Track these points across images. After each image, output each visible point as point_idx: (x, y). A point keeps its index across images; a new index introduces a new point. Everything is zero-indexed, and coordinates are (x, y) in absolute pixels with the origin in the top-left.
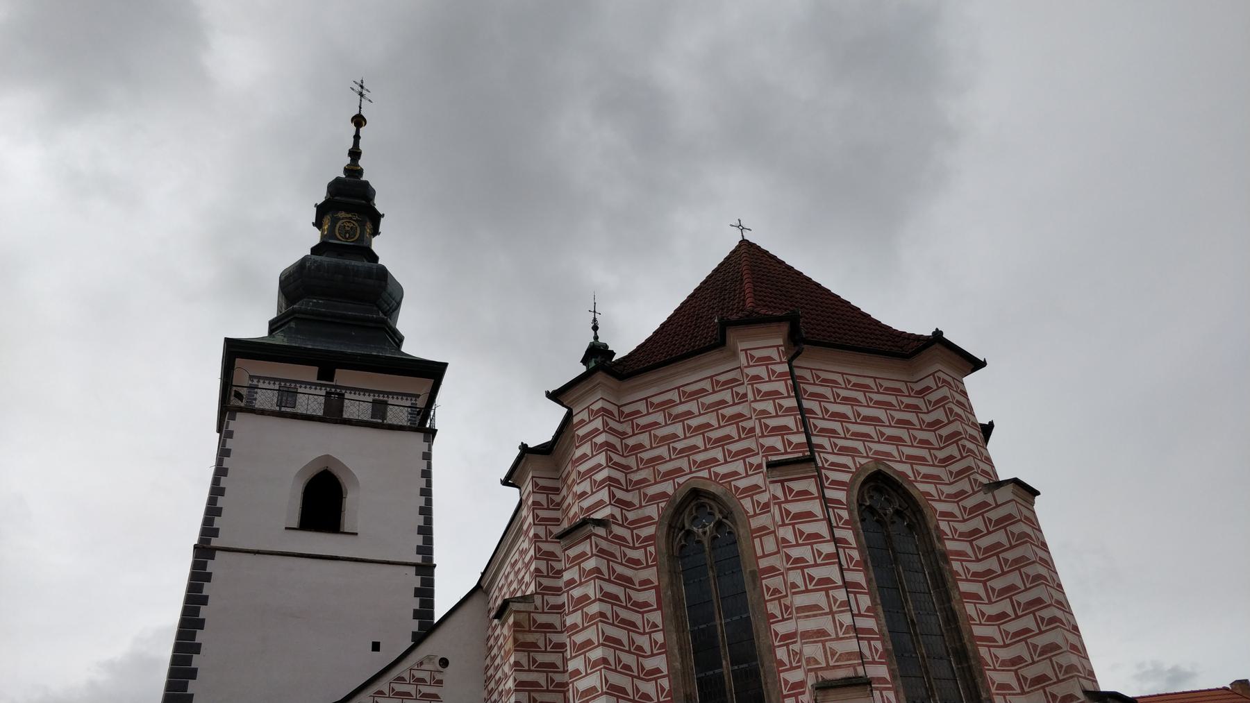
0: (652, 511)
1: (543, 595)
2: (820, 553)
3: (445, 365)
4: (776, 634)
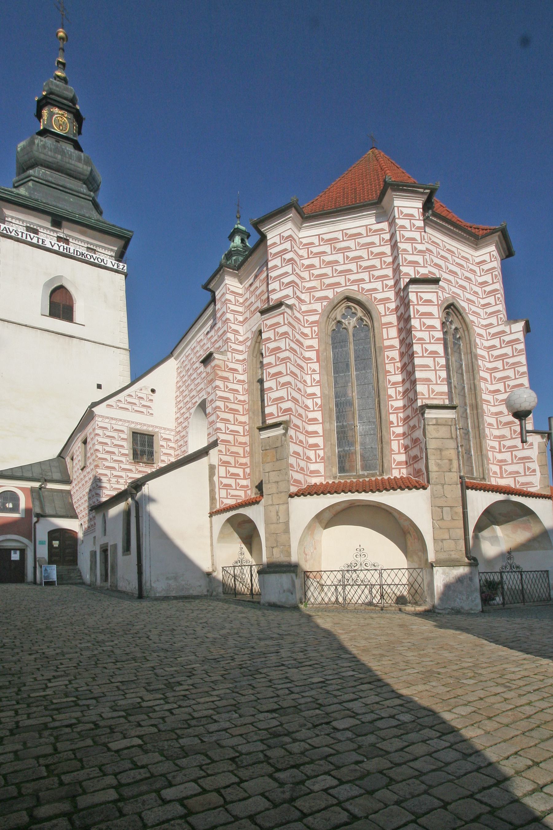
0: (318, 307)
2: (433, 337)
4: (390, 382)
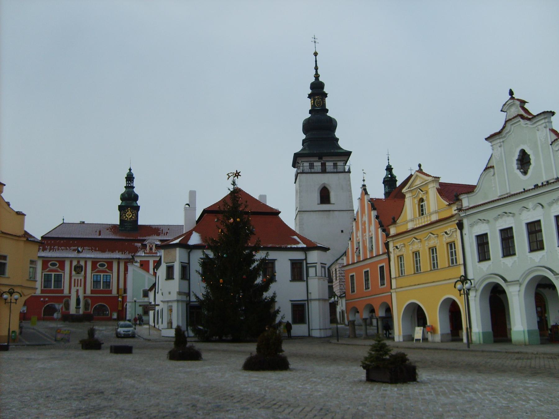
3: (351, 152)
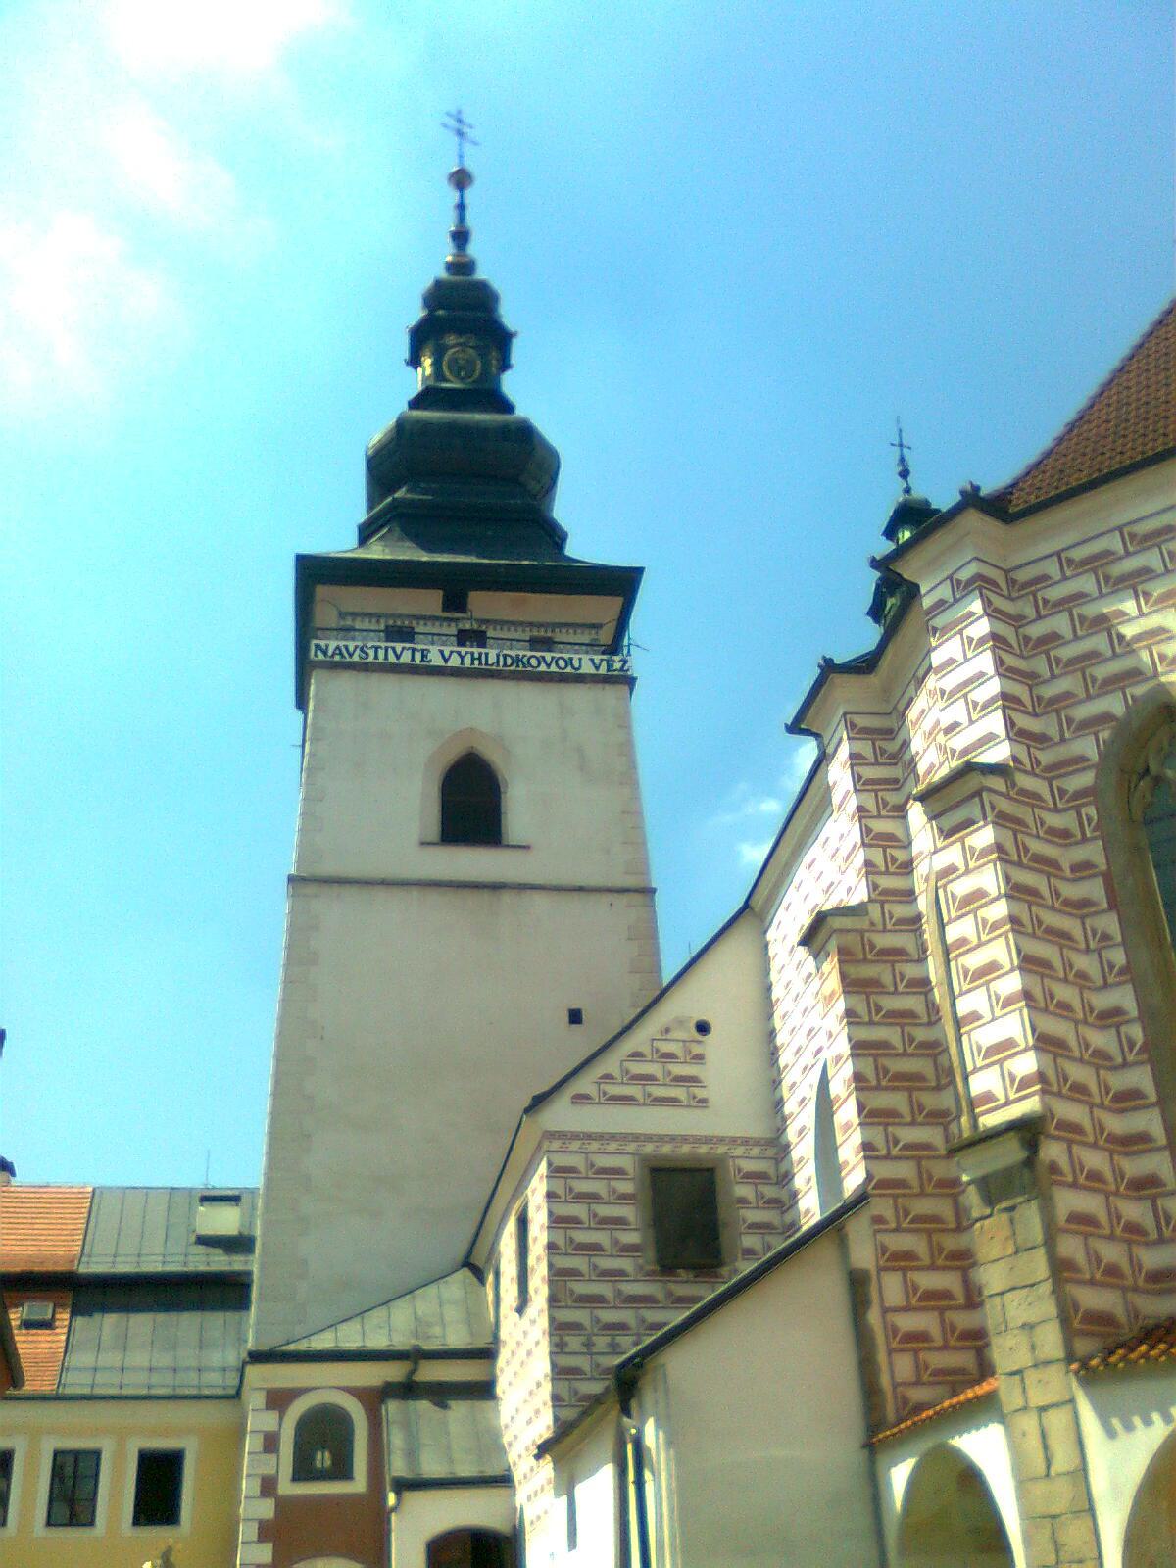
0: (1087, 747)
1: (882, 903)
3: (639, 571)
